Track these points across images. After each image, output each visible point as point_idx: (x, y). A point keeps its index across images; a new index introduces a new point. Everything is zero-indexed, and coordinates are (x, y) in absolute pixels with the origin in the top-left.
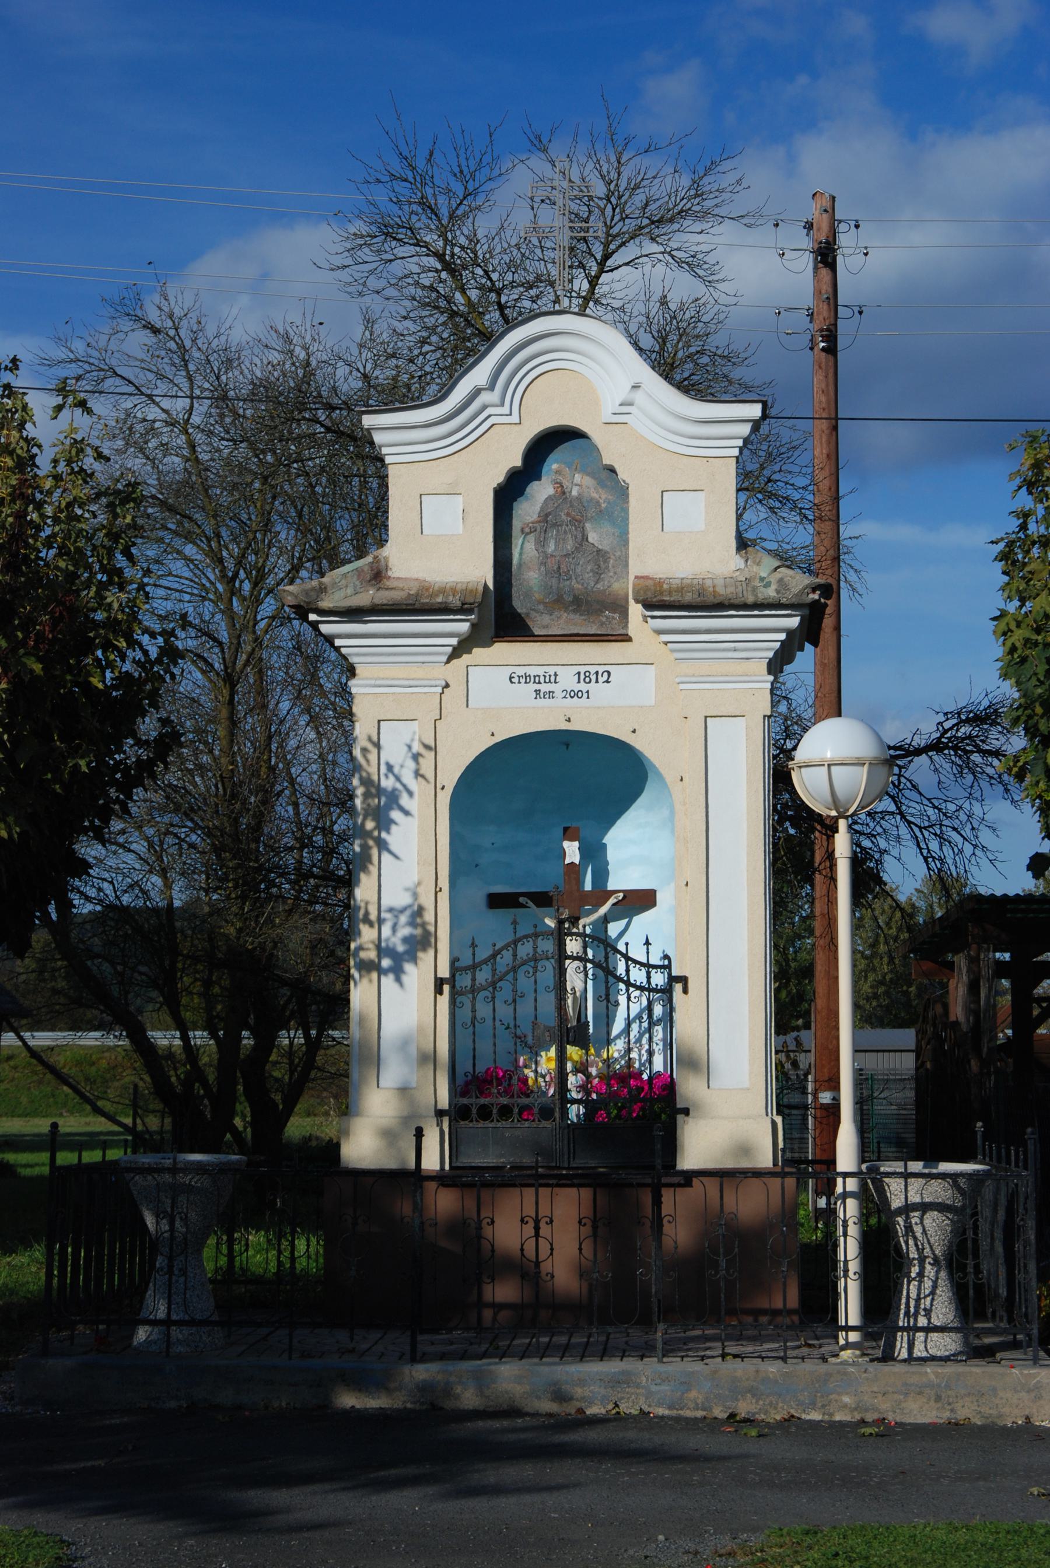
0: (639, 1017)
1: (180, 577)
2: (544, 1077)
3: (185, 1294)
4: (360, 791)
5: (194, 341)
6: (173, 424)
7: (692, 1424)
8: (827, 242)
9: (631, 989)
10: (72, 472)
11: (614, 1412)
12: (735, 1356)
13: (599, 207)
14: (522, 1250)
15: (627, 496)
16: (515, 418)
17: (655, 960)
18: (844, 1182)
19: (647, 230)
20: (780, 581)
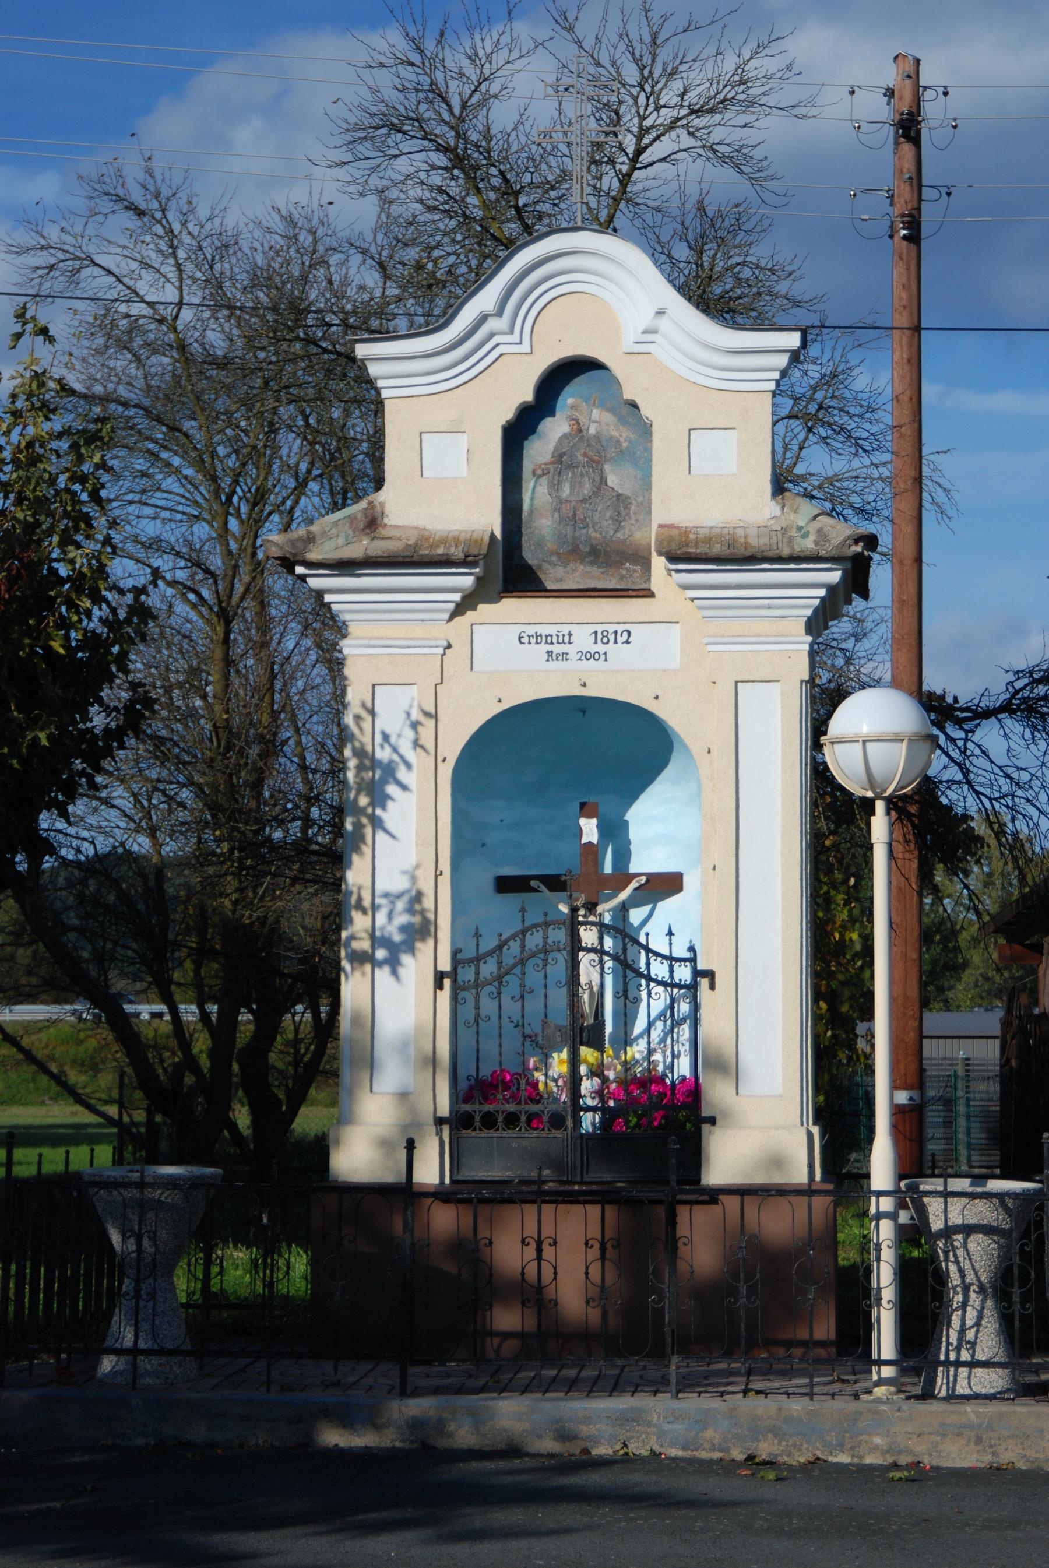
0: (661, 1016)
1: (170, 493)
2: (556, 1081)
3: (153, 1320)
4: (352, 763)
5: (184, 224)
6: (161, 321)
7: (705, 1467)
8: (910, 114)
9: (652, 984)
10: (33, 408)
11: (622, 1452)
12: (758, 1392)
13: (631, 95)
14: (523, 1274)
15: (651, 434)
16: (525, 347)
17: (681, 951)
18: (878, 1202)
19: (684, 122)
20: (820, 531)
